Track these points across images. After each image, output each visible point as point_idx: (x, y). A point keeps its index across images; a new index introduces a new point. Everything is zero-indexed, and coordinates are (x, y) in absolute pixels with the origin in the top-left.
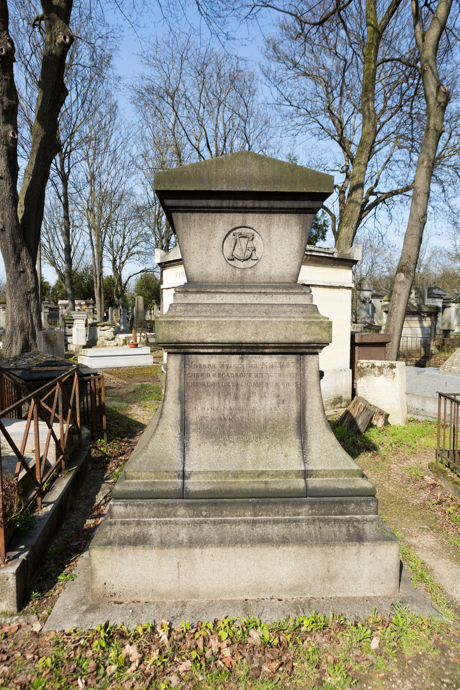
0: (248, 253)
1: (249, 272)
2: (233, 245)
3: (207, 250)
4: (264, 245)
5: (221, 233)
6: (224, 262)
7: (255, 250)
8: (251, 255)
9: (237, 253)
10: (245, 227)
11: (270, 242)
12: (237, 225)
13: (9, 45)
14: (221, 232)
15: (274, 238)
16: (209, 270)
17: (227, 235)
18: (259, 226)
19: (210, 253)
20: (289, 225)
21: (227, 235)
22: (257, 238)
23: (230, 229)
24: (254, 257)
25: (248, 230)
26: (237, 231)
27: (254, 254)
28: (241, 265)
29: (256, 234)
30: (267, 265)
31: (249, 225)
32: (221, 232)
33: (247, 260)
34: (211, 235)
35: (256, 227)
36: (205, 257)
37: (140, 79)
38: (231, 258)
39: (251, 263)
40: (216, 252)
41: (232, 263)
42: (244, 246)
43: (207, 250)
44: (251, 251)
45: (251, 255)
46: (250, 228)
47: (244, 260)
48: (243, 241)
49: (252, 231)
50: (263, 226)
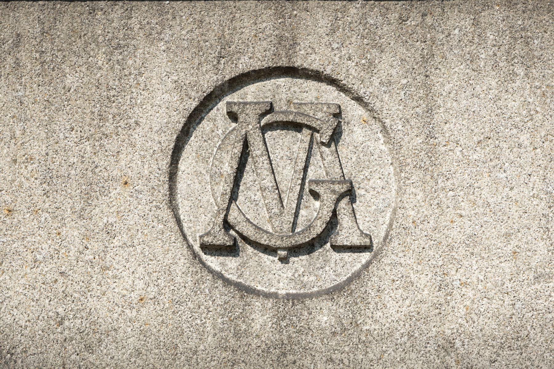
0: (314, 213)
1: (324, 315)
2: (228, 168)
3: (87, 198)
4: (401, 166)
5: (160, 107)
6: (183, 261)
7: (350, 194)
8: (333, 223)
9: (256, 210)
10: (291, 71)
11: (432, 152)
12: (245, 64)
13: (264, 194)
14: (161, 97)
15: (452, 127)
16: (100, 308)
17: (195, 118)
18: (370, 67)
19: (103, 213)
20: (529, 60)
21: (195, 118)
22: (356, 134)
23: (208, 81)
24: (346, 234)
25: (310, 91)
26: (251, 92)
27: (345, 220)
28: (277, 276)
29: (353, 111)
30: (423, 280)
31: (314, 62)
32: (161, 97)
33: (309, 247)
34: (108, 114)
35: (349, 74)
36: (73, 233)
37: (11, 207)
38: (222, 239)
39: (332, 267)
40: (132, 208)
41: (228, 266)
42: (288, 175)
43: (87, 198)
44: (328, 198)
45: (333, 223)
46: (317, 76)
47: (296, 250)
48: (286, 147)
49: (331, 95)
50: (388, 65)
